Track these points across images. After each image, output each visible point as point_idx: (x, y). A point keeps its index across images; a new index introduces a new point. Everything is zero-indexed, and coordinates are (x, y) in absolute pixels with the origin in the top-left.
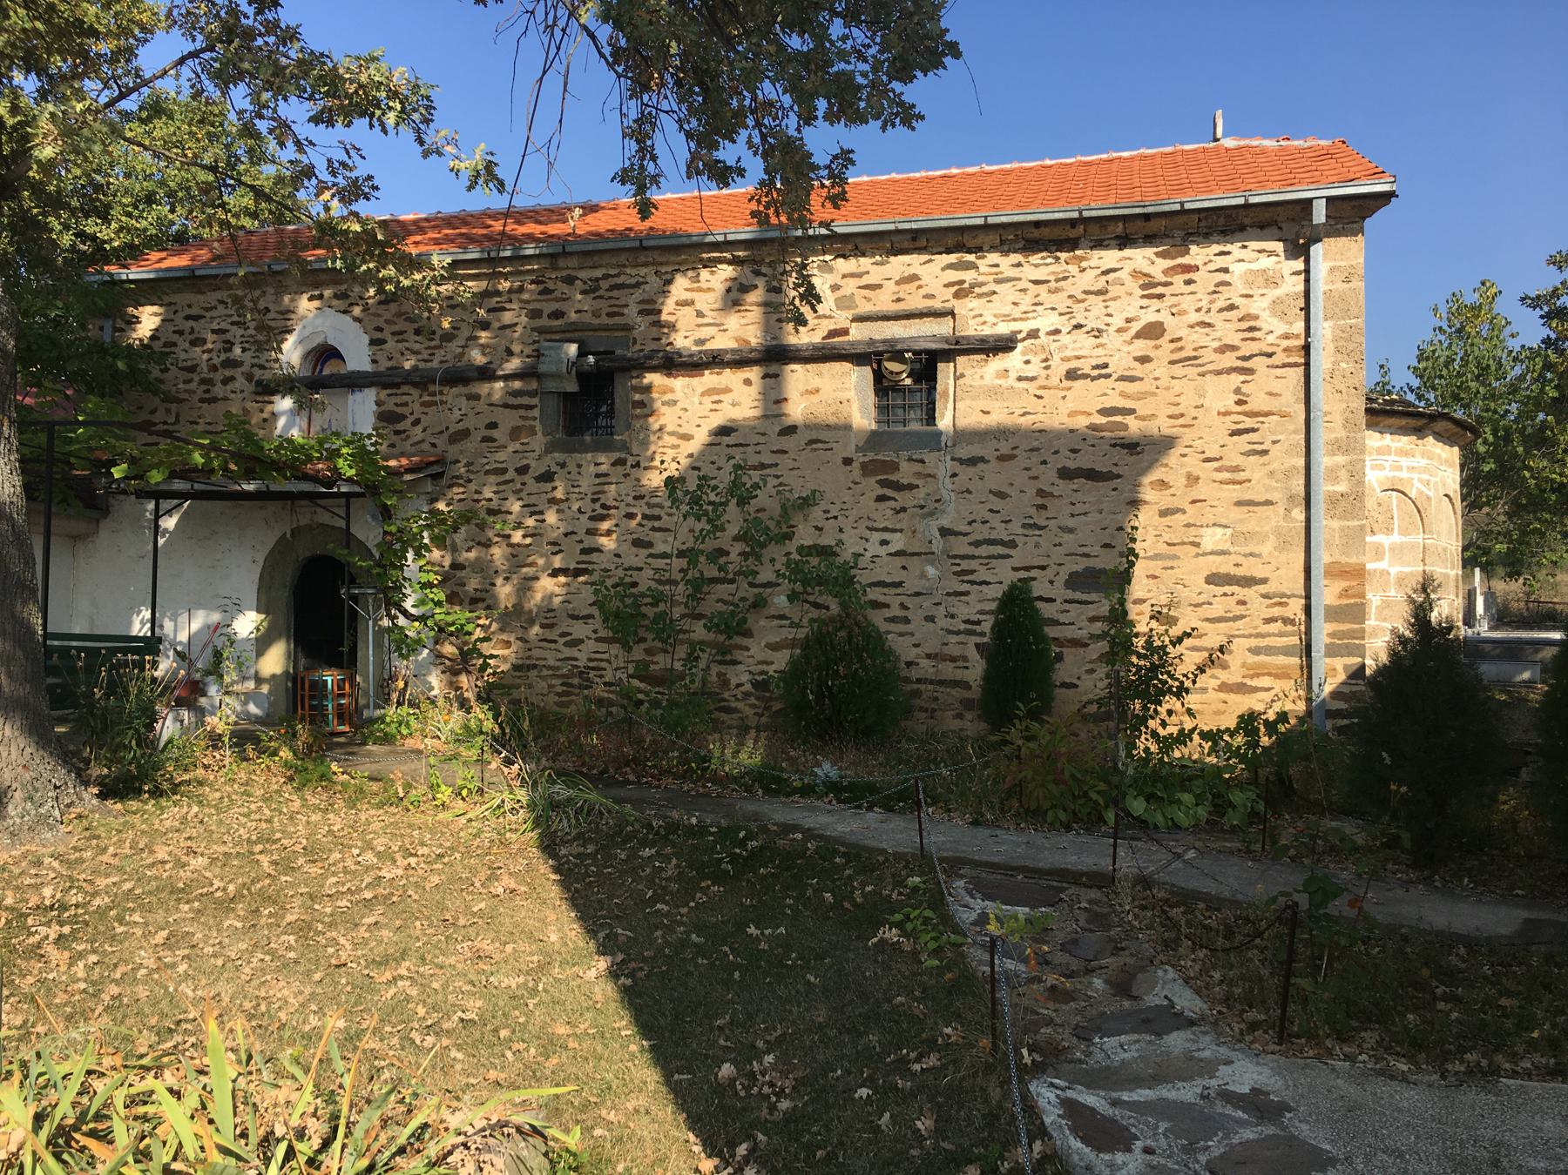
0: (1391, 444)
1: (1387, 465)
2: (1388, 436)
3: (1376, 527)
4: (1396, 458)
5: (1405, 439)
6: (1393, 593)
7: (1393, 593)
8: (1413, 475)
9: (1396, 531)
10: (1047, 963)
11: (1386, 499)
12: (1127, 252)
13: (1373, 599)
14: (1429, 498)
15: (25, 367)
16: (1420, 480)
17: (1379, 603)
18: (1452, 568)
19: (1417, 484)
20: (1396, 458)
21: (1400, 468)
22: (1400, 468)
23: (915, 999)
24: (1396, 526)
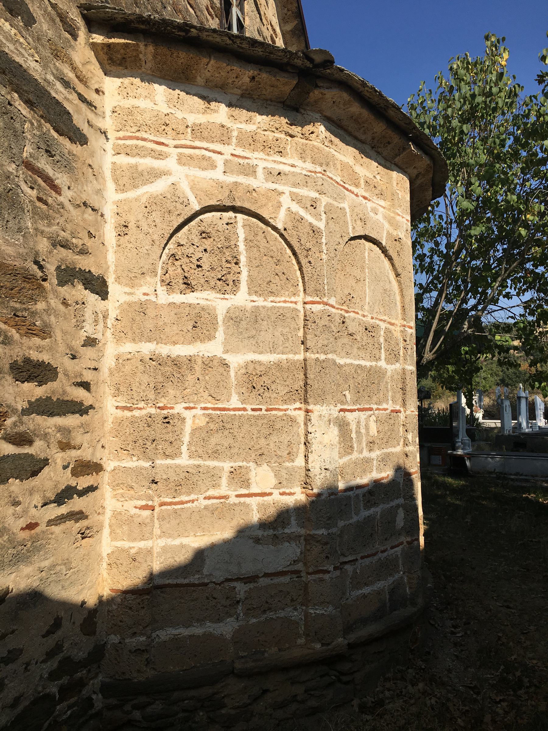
0: (228, 123)
1: (219, 160)
2: (223, 108)
3: (195, 277)
4: (239, 151)
5: (261, 120)
6: (235, 402)
7: (235, 402)
8: (280, 188)
9: (244, 286)
10: (277, 275)
11: (221, 225)
12: (231, 204)
13: (188, 414)
14: (315, 231)
15: (487, 267)
16: (294, 197)
17: (202, 422)
18: (393, 357)
19: (286, 201)
20: (239, 151)
21: (251, 171)
22: (251, 171)
23: (455, 133)
24: (244, 277)
